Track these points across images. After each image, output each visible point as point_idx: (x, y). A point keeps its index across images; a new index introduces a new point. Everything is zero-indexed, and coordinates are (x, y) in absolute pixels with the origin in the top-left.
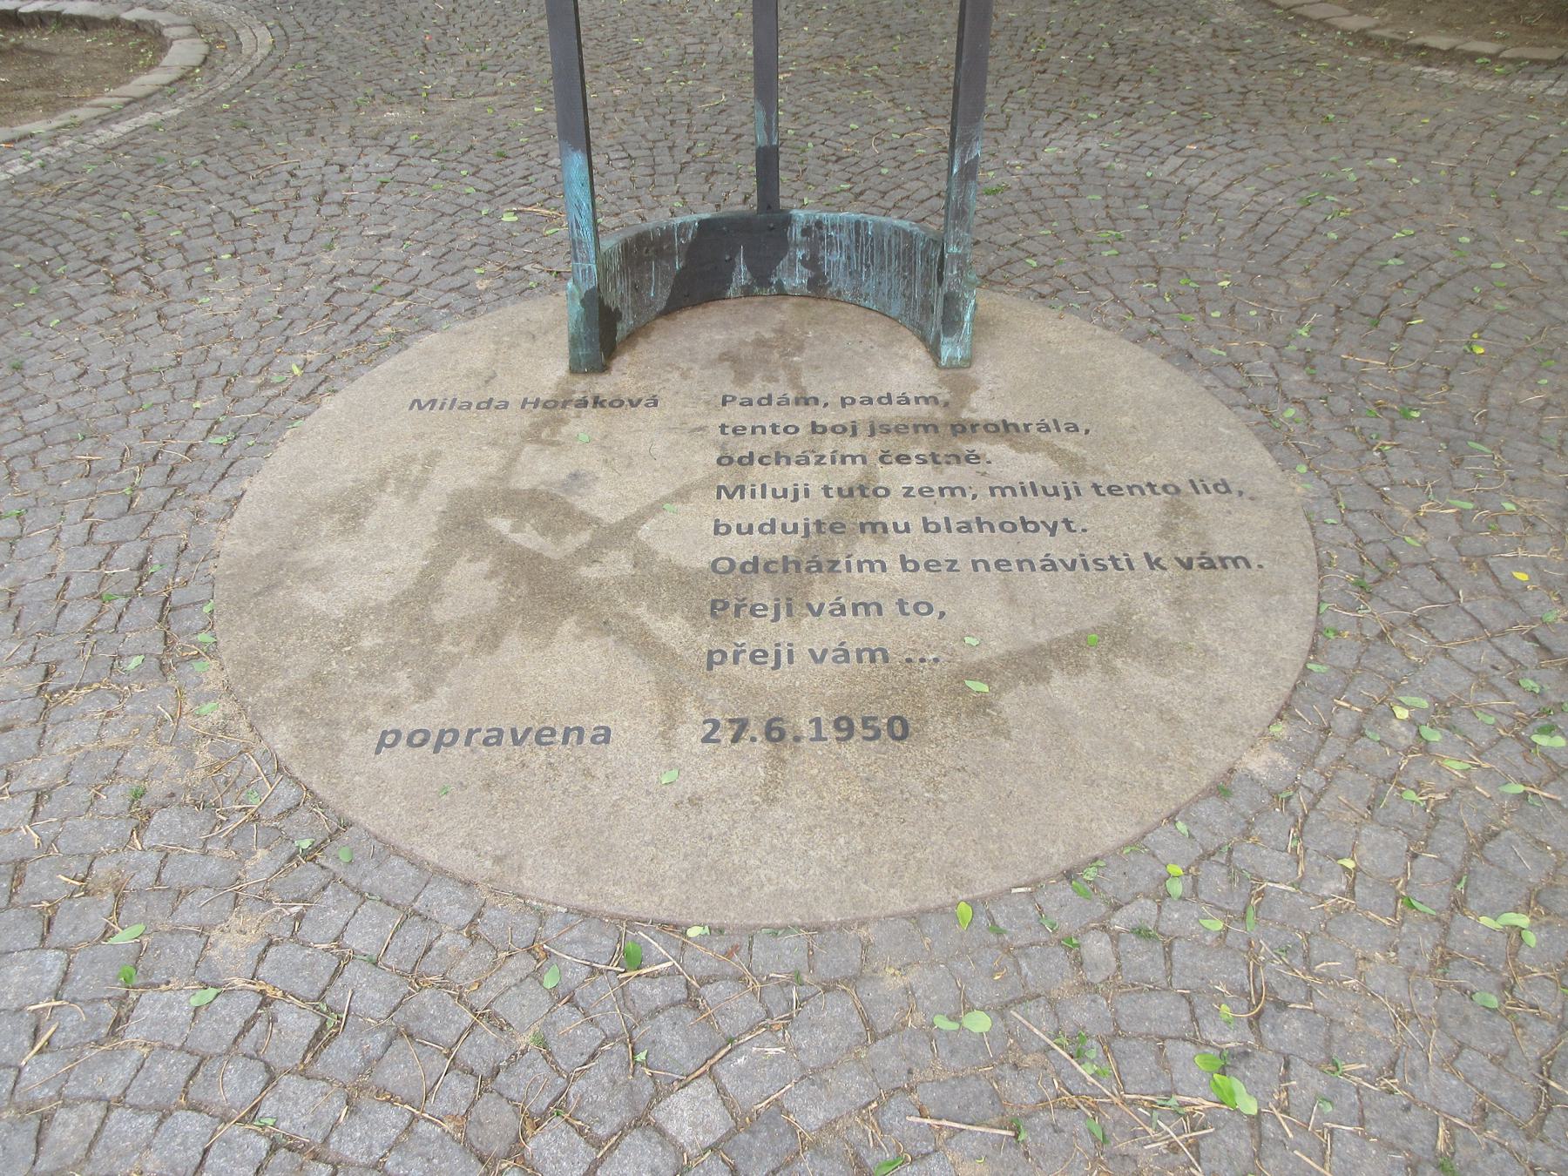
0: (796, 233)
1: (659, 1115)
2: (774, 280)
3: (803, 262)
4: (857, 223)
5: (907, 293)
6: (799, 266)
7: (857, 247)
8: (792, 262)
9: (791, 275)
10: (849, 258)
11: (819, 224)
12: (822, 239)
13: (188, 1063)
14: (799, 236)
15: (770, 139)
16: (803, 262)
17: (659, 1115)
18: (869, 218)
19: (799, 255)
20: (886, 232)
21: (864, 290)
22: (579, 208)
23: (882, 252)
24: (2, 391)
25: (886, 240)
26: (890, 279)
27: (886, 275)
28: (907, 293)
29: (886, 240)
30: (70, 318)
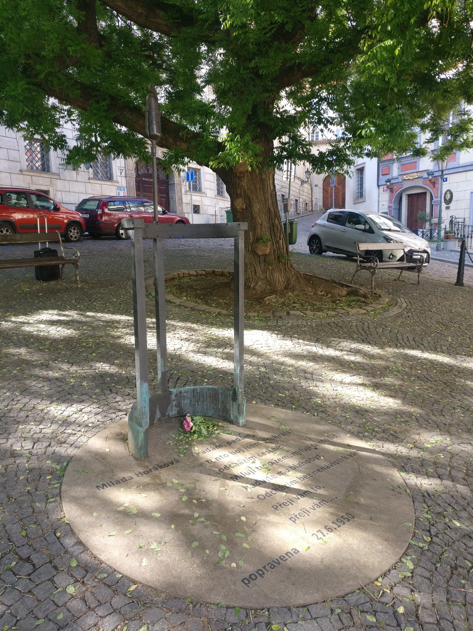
0: (173, 397)
1: (55, 579)
2: (167, 414)
3: (176, 406)
4: (194, 390)
5: (215, 407)
6: (174, 408)
7: (194, 397)
8: (172, 407)
9: (172, 411)
10: (191, 401)
11: (180, 392)
12: (181, 397)
13: (449, 96)
14: (174, 398)
15: (165, 369)
16: (176, 406)
17: (55, 579)
18: (197, 387)
19: (174, 404)
20: (205, 390)
21: (196, 410)
22: (145, 401)
23: (204, 396)
24: (1, 434)
25: (205, 393)
26: (207, 404)
27: (205, 403)
28: (215, 407)
29: (205, 393)
30: (81, 411)
